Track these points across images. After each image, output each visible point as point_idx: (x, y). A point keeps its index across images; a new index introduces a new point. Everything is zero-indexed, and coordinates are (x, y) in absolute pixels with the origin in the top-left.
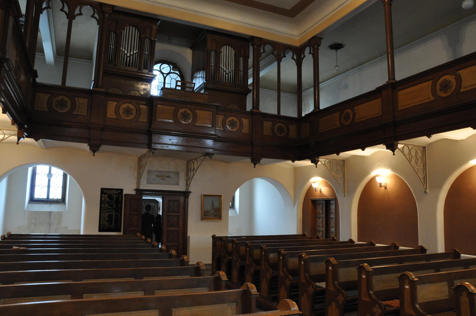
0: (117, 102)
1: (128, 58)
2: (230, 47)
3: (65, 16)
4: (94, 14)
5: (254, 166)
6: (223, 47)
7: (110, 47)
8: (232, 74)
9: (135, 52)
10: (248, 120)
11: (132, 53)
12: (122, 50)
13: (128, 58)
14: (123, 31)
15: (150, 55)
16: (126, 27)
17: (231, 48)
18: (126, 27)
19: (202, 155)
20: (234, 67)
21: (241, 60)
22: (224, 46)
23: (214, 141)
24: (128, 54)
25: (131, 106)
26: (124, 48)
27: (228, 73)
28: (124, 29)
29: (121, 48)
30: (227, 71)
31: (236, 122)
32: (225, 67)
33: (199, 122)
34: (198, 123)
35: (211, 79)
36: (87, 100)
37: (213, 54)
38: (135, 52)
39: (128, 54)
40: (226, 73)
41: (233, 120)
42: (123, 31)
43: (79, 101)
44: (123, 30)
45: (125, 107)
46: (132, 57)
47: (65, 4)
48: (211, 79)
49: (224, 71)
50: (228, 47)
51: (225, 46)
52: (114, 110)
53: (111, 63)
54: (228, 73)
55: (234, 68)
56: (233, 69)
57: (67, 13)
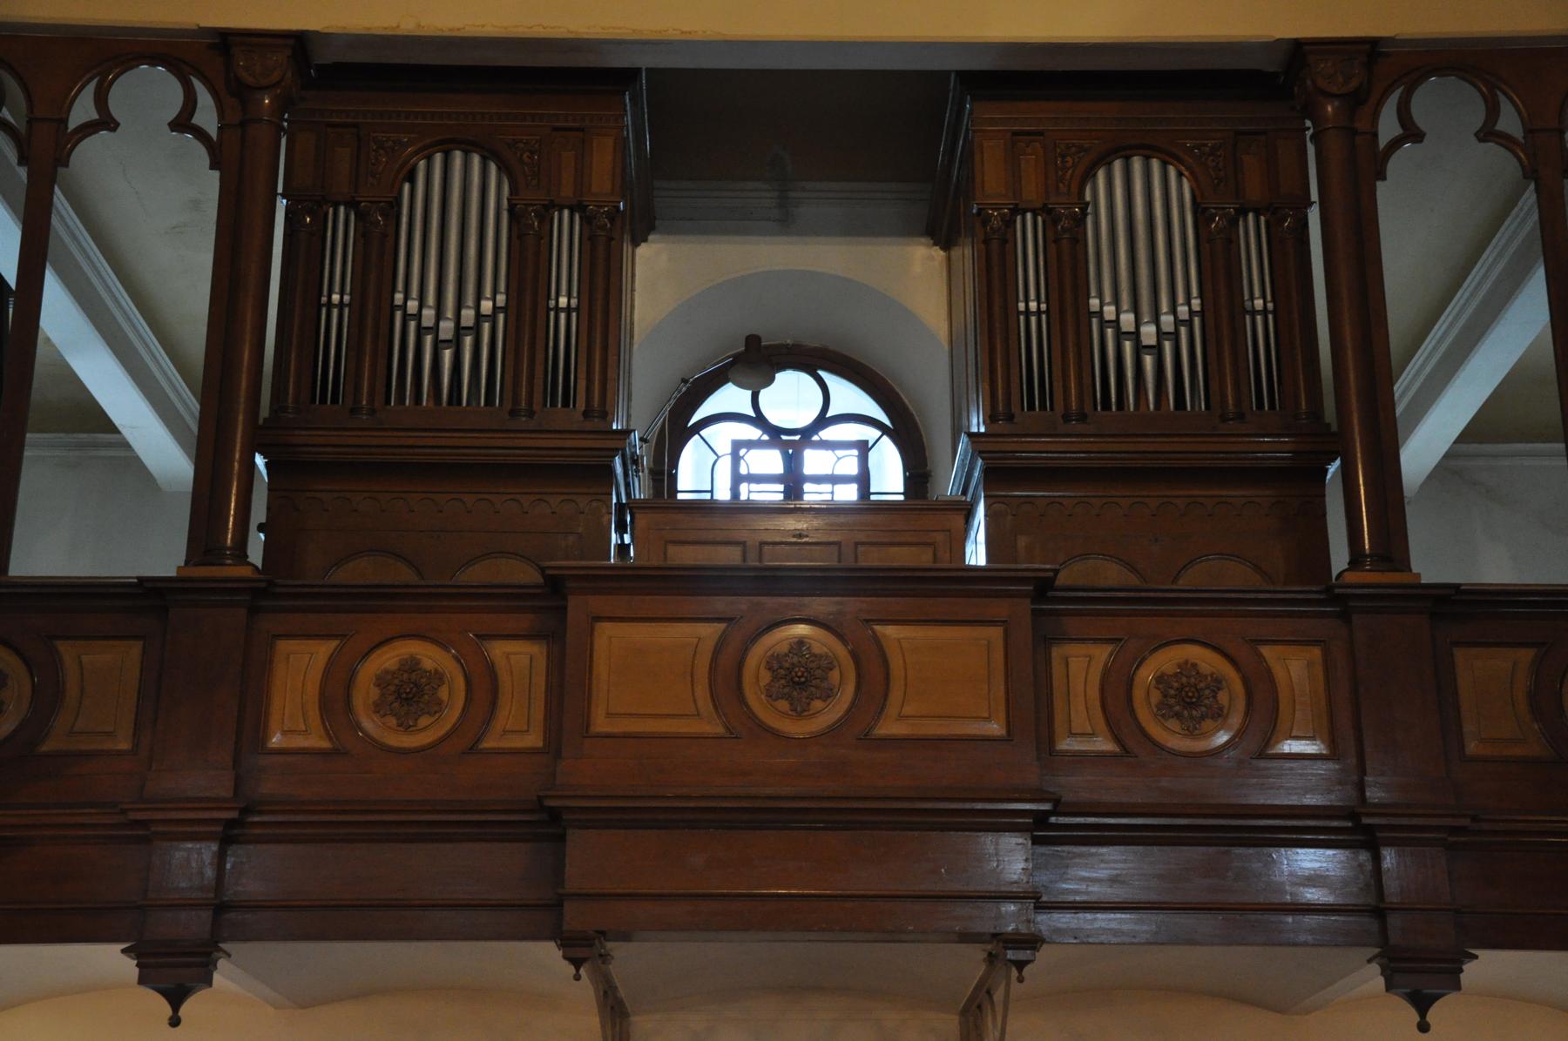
0: (334, 637)
1: (447, 354)
2: (1155, 165)
3: (201, 154)
4: (88, 129)
5: (1417, 1019)
6: (1101, 175)
7: (324, 299)
8: (1191, 343)
9: (486, 306)
10: (1316, 653)
11: (468, 316)
12: (1100, 313)
13: (447, 354)
14: (407, 187)
15: (585, 311)
16: (422, 164)
17: (1164, 164)
18: (422, 164)
19: (975, 955)
20: (1195, 292)
21: (1251, 234)
22: (1105, 160)
23: (1036, 841)
24: (442, 324)
25: (430, 656)
26: (414, 292)
27: (1153, 341)
28: (411, 178)
29: (399, 297)
30: (1148, 333)
31: (1218, 683)
32: (1108, 299)
33: (907, 710)
34: (901, 717)
35: (1260, 405)
36: (136, 648)
37: (1028, 231)
38: (486, 306)
39: (1148, 333)
40: (1139, 350)
41: (1187, 667)
42: (407, 187)
43: (81, 662)
44: (404, 180)
45: (387, 665)
46: (468, 341)
47: (198, 85)
48: (1260, 405)
49: (1120, 336)
50: (1137, 164)
51: (1118, 165)
52: (313, 689)
53: (566, 404)
54: (1153, 341)
55: (1196, 304)
56: (1191, 312)
57: (213, 133)
